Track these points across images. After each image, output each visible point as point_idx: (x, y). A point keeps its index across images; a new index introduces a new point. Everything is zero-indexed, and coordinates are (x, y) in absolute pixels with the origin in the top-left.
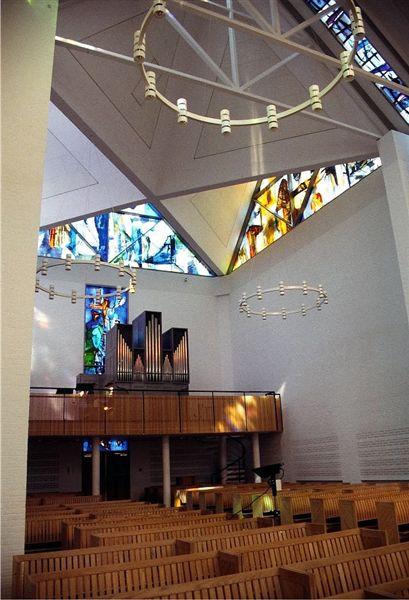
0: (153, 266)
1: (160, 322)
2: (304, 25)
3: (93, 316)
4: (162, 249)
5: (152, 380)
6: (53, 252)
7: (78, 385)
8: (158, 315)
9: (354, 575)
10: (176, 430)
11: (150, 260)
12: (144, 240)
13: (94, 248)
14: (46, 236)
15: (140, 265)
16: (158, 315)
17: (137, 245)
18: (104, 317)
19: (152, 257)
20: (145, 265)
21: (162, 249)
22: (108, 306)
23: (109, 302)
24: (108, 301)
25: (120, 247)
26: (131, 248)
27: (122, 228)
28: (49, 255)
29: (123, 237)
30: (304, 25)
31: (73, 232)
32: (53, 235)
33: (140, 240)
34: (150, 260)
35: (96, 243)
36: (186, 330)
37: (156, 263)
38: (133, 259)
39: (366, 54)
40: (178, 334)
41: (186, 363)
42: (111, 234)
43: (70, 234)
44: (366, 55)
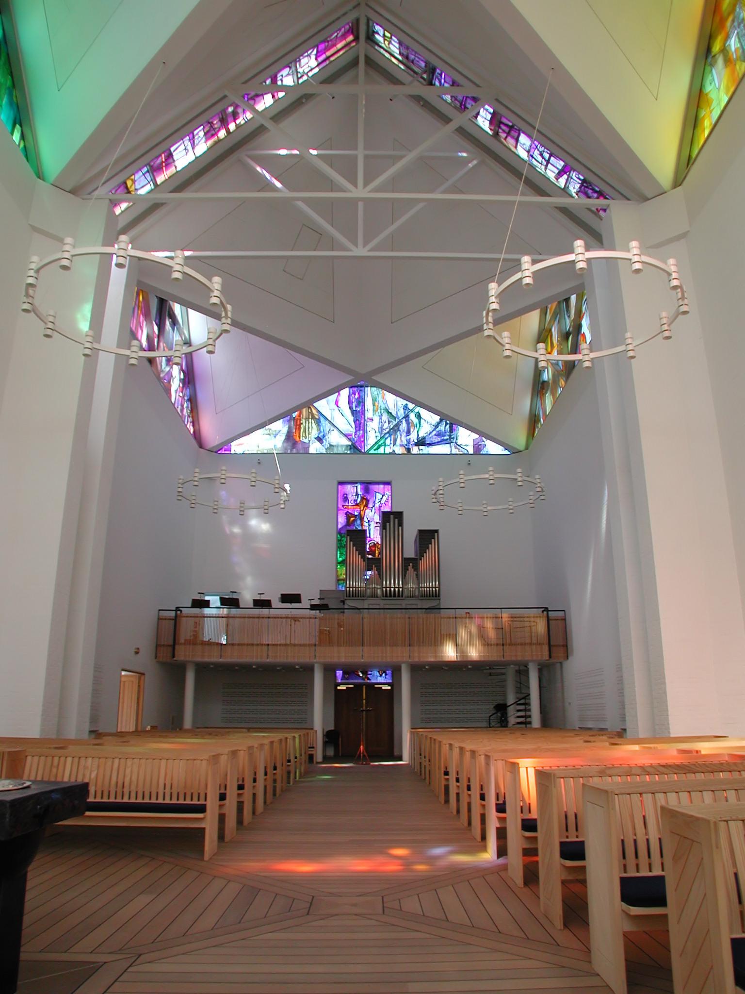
0: (425, 450)
1: (401, 524)
2: (453, 125)
3: (348, 518)
4: (437, 426)
5: (389, 595)
6: (300, 446)
7: (255, 601)
8: (399, 515)
9: (120, 785)
10: (199, 659)
11: (421, 442)
12: (412, 417)
13: (347, 436)
14: (289, 428)
15: (409, 450)
16: (399, 515)
17: (404, 425)
18: (362, 519)
19: (424, 438)
20: (415, 450)
21: (437, 426)
22: (367, 505)
23: (368, 501)
24: (366, 502)
25: (381, 429)
26: (395, 429)
27: (383, 406)
28: (294, 451)
29: (385, 417)
30: (453, 125)
31: (322, 419)
32: (298, 426)
33: (407, 417)
34: (421, 442)
35: (350, 429)
36: (437, 531)
37: (430, 445)
38: (398, 442)
39: (541, 154)
40: (427, 537)
41: (437, 572)
42: (369, 414)
43: (318, 422)
44: (543, 158)
